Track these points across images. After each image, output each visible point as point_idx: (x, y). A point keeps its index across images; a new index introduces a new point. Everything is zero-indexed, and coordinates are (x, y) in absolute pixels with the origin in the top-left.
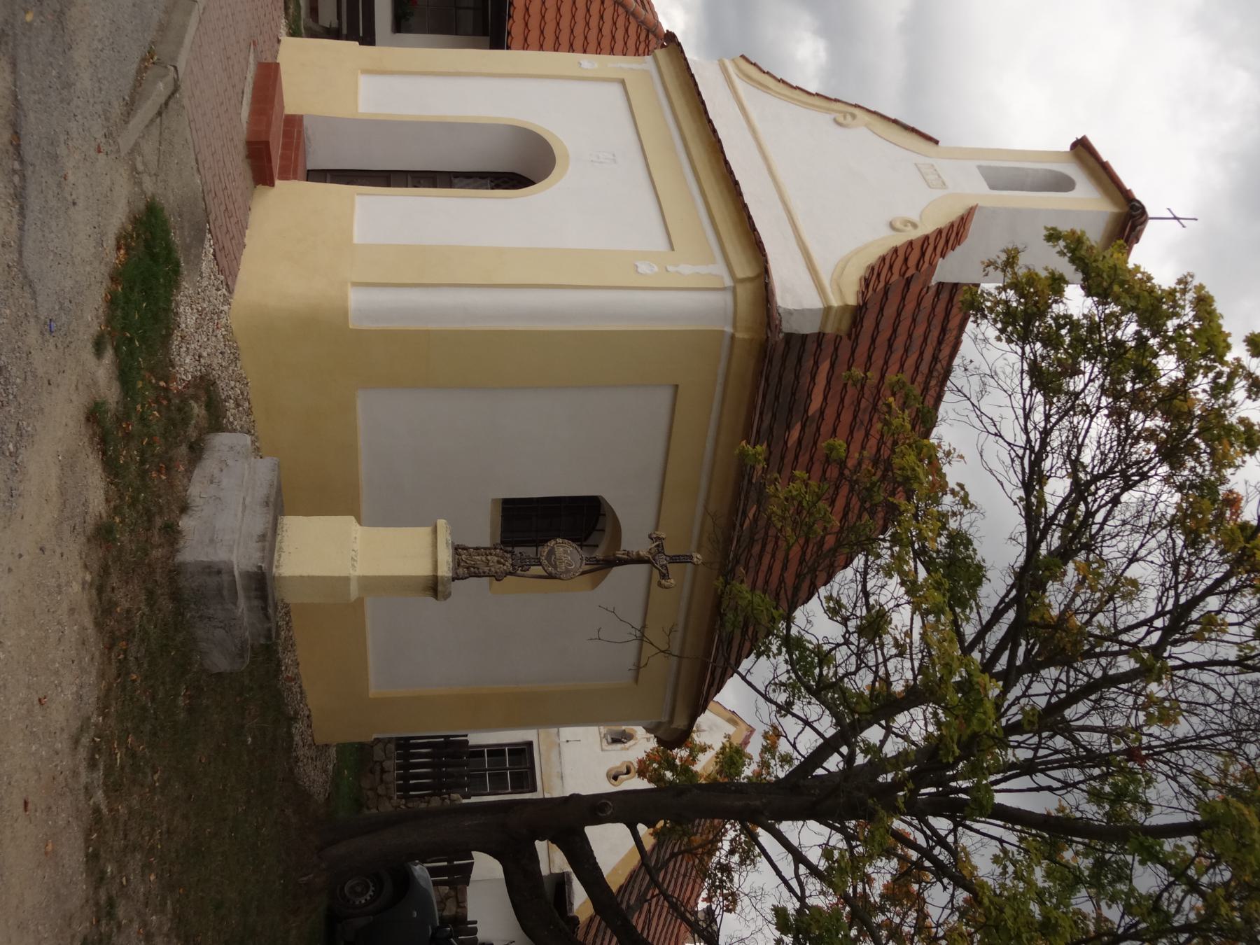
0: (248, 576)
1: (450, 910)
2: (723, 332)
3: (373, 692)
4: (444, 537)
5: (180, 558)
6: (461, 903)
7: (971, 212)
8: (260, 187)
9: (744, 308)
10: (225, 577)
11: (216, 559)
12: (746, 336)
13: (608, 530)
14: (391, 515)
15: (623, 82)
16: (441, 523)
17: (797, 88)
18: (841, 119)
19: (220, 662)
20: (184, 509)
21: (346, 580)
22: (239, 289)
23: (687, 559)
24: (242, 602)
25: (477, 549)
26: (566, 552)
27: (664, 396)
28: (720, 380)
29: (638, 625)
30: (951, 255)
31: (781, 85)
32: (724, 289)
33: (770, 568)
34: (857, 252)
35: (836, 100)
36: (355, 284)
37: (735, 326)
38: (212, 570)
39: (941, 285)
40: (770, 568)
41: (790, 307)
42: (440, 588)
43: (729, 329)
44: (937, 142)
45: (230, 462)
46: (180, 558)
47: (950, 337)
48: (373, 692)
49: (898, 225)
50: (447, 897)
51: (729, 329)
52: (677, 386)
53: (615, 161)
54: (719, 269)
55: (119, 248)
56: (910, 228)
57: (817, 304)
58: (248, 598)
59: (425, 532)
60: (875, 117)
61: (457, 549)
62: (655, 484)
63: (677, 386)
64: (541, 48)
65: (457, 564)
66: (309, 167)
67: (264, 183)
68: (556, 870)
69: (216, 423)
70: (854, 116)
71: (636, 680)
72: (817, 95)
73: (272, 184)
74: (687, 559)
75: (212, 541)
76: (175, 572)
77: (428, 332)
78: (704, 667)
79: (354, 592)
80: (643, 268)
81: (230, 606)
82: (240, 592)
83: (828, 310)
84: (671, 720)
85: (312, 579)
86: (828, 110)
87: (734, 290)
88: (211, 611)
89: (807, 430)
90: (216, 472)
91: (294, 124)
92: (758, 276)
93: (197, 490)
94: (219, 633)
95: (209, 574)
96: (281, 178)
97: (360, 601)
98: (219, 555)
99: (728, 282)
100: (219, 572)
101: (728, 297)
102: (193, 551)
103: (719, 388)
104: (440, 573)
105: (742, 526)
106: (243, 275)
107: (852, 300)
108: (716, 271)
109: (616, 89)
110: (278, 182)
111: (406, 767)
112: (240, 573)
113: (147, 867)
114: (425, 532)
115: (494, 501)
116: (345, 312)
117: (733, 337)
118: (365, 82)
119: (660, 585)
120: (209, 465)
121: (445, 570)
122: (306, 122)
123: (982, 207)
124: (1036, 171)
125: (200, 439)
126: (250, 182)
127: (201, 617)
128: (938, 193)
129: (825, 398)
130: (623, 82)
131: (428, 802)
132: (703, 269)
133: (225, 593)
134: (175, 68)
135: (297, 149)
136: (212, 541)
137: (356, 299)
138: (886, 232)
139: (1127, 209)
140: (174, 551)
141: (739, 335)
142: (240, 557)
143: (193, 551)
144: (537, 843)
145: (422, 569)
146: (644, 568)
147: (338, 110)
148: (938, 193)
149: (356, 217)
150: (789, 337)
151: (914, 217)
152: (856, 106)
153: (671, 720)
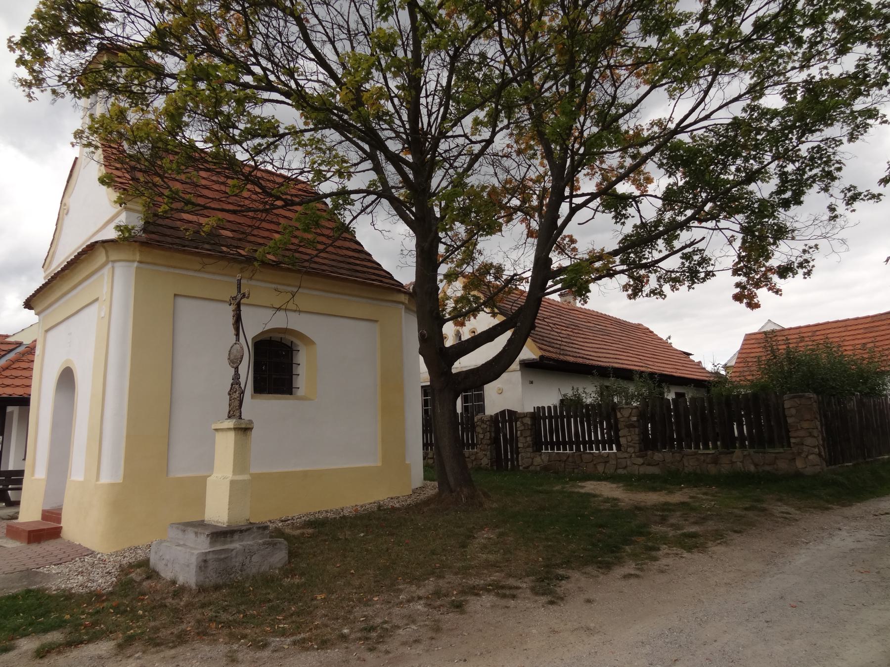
1: (528, 421)
2: (137, 268)
3: (379, 464)
6: (525, 415)
8: (61, 535)
9: (122, 256)
10: (210, 557)
11: (195, 563)
13: (282, 336)
21: (232, 483)
27: (181, 301)
28: (172, 270)
29: (271, 312)
32: (113, 267)
37: (133, 261)
38: (204, 564)
44: (76, 158)
46: (194, 586)
48: (379, 464)
50: (522, 422)
51: (136, 264)
52: (175, 295)
54: (106, 271)
58: (231, 542)
62: (206, 303)
63: (175, 295)
67: (60, 532)
68: (518, 367)
71: (376, 321)
76: (202, 589)
78: (308, 273)
81: (234, 553)
82: (226, 547)
84: (403, 303)
85: (230, 503)
86: (63, 219)
87: (114, 261)
88: (237, 564)
92: (104, 248)
94: (255, 558)
95: (206, 567)
97: (251, 475)
99: (110, 265)
101: (117, 265)
102: (188, 577)
103: (177, 271)
106: (89, 546)
109: (51, 334)
111: (558, 443)
112: (211, 547)
117: (140, 262)
119: (248, 298)
122: (47, 508)
126: (58, 541)
127: (241, 571)
130: (47, 331)
131: (630, 426)
132: (106, 277)
135: (52, 513)
137: (106, 479)
143: (188, 577)
144: (454, 371)
146: (242, 308)
150: (144, 230)
153: (403, 303)
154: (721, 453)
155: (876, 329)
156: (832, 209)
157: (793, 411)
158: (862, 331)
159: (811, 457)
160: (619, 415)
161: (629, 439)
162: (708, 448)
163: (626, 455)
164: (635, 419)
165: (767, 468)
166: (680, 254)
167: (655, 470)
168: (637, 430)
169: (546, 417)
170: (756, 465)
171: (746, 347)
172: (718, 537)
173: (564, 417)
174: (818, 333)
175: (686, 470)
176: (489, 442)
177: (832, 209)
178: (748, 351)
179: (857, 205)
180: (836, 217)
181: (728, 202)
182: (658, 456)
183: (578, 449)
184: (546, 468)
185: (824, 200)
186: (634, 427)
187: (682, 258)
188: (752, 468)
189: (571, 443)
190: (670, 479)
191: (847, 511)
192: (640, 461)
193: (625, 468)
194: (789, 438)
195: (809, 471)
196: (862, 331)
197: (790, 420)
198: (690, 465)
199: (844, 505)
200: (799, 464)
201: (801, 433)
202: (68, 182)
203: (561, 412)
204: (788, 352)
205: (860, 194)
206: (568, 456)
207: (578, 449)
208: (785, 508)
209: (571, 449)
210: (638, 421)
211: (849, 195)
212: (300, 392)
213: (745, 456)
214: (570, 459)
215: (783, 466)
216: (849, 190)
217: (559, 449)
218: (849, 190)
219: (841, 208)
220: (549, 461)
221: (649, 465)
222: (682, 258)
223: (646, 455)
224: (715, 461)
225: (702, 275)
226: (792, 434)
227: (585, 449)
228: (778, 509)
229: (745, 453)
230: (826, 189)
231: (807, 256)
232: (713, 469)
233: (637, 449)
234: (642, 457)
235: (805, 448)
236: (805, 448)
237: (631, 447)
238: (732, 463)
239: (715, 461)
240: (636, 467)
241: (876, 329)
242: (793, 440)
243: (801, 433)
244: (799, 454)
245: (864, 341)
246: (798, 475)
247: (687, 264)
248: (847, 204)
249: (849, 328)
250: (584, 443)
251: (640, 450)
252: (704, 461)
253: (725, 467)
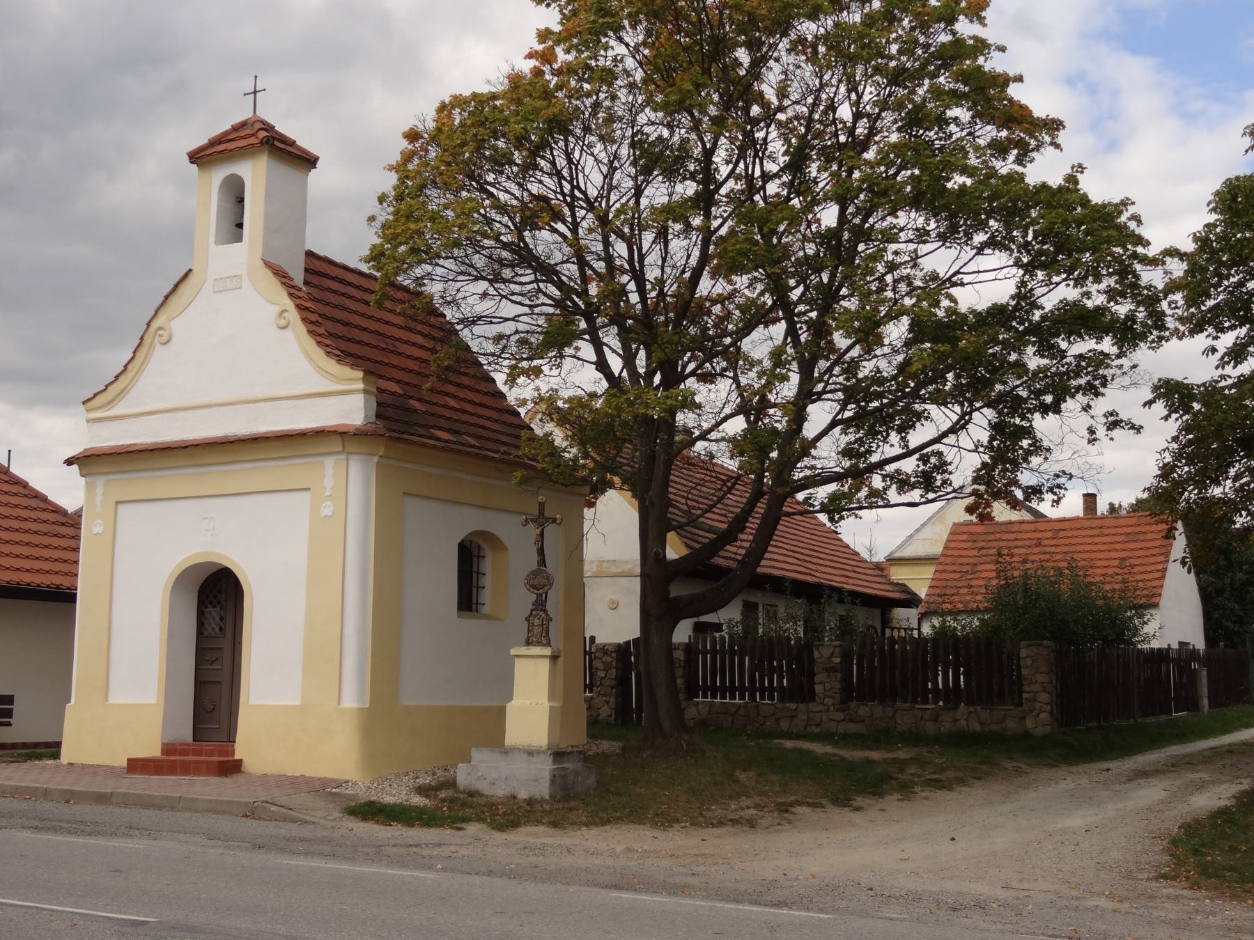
0: (554, 762)
4: (523, 650)
5: (547, 797)
14: (505, 685)
15: (118, 503)
16: (513, 652)
18: (164, 339)
20: (514, 797)
30: (291, 275)
33: (489, 419)
34: (311, 360)
35: (142, 338)
36: (339, 703)
40: (489, 419)
43: (376, 459)
46: (547, 797)
56: (285, 315)
59: (517, 662)
65: (539, 643)
69: (451, 784)
70: (160, 328)
73: (241, 761)
74: (542, 505)
75: (536, 780)
80: (327, 511)
83: (365, 391)
86: (151, 346)
91: (168, 749)
93: (500, 792)
94: (580, 779)
96: (233, 753)
98: (546, 775)
101: (352, 457)
105: (473, 446)
107: (360, 374)
108: (329, 463)
110: (237, 757)
111: (723, 690)
113: (709, 810)
114: (517, 662)
115: (459, 616)
116: (361, 709)
118: (118, 696)
120: (483, 787)
121: (547, 651)
125: (464, 792)
128: (246, 283)
129: (389, 379)
130: (118, 503)
131: (830, 670)
136: (536, 780)
138: (288, 333)
142: (545, 767)
145: (545, 665)
147: (158, 717)
152: (148, 324)
154: (942, 708)
155: (1142, 537)
156: (1091, 431)
157: (1029, 661)
158: (1121, 538)
159: (1043, 715)
160: (816, 654)
161: (828, 686)
162: (927, 703)
163: (821, 708)
164: (838, 660)
165: (995, 728)
166: (917, 456)
167: (854, 728)
168: (839, 675)
169: (707, 652)
170: (982, 724)
171: (953, 545)
172: (961, 782)
173: (707, 652)
174: (1062, 534)
175: (899, 728)
176: (614, 683)
177: (1091, 431)
178: (957, 553)
179: (1117, 433)
180: (1095, 440)
181: (974, 390)
182: (864, 710)
183: (753, 698)
184: (703, 724)
185: (1084, 421)
186: (835, 671)
187: (918, 460)
188: (978, 728)
189: (742, 690)
190: (882, 737)
191: (1073, 769)
192: (841, 716)
193: (819, 725)
194: (1021, 692)
195: (1040, 731)
196: (1121, 538)
197: (1024, 672)
198: (904, 721)
199: (1070, 765)
200: (1029, 723)
201: (1035, 688)
202: (167, 298)
203: (731, 646)
204: (1026, 577)
205: (1122, 421)
206: (739, 707)
207: (753, 698)
208: (1015, 764)
209: (742, 698)
210: (841, 663)
211: (1110, 419)
212: (486, 610)
213: (970, 713)
214: (742, 712)
215: (1011, 725)
216: (1111, 415)
217: (723, 697)
218: (1111, 415)
219: (1101, 432)
220: (709, 713)
221: (851, 721)
222: (918, 460)
223: (849, 708)
224: (935, 719)
225: (938, 483)
226: (1025, 688)
227: (762, 698)
228: (1009, 765)
229: (971, 709)
230: (1087, 408)
231: (1062, 480)
232: (930, 728)
233: (838, 701)
234: (843, 711)
235: (1037, 705)
236: (1037, 705)
237: (829, 697)
238: (955, 720)
239: (935, 719)
240: (834, 725)
241: (1142, 537)
242: (1025, 696)
243: (1035, 688)
244: (1031, 711)
245: (1123, 555)
246: (1027, 735)
247: (922, 467)
248: (1109, 429)
249: (1106, 531)
250: (763, 690)
251: (842, 702)
252: (922, 718)
253: (946, 725)
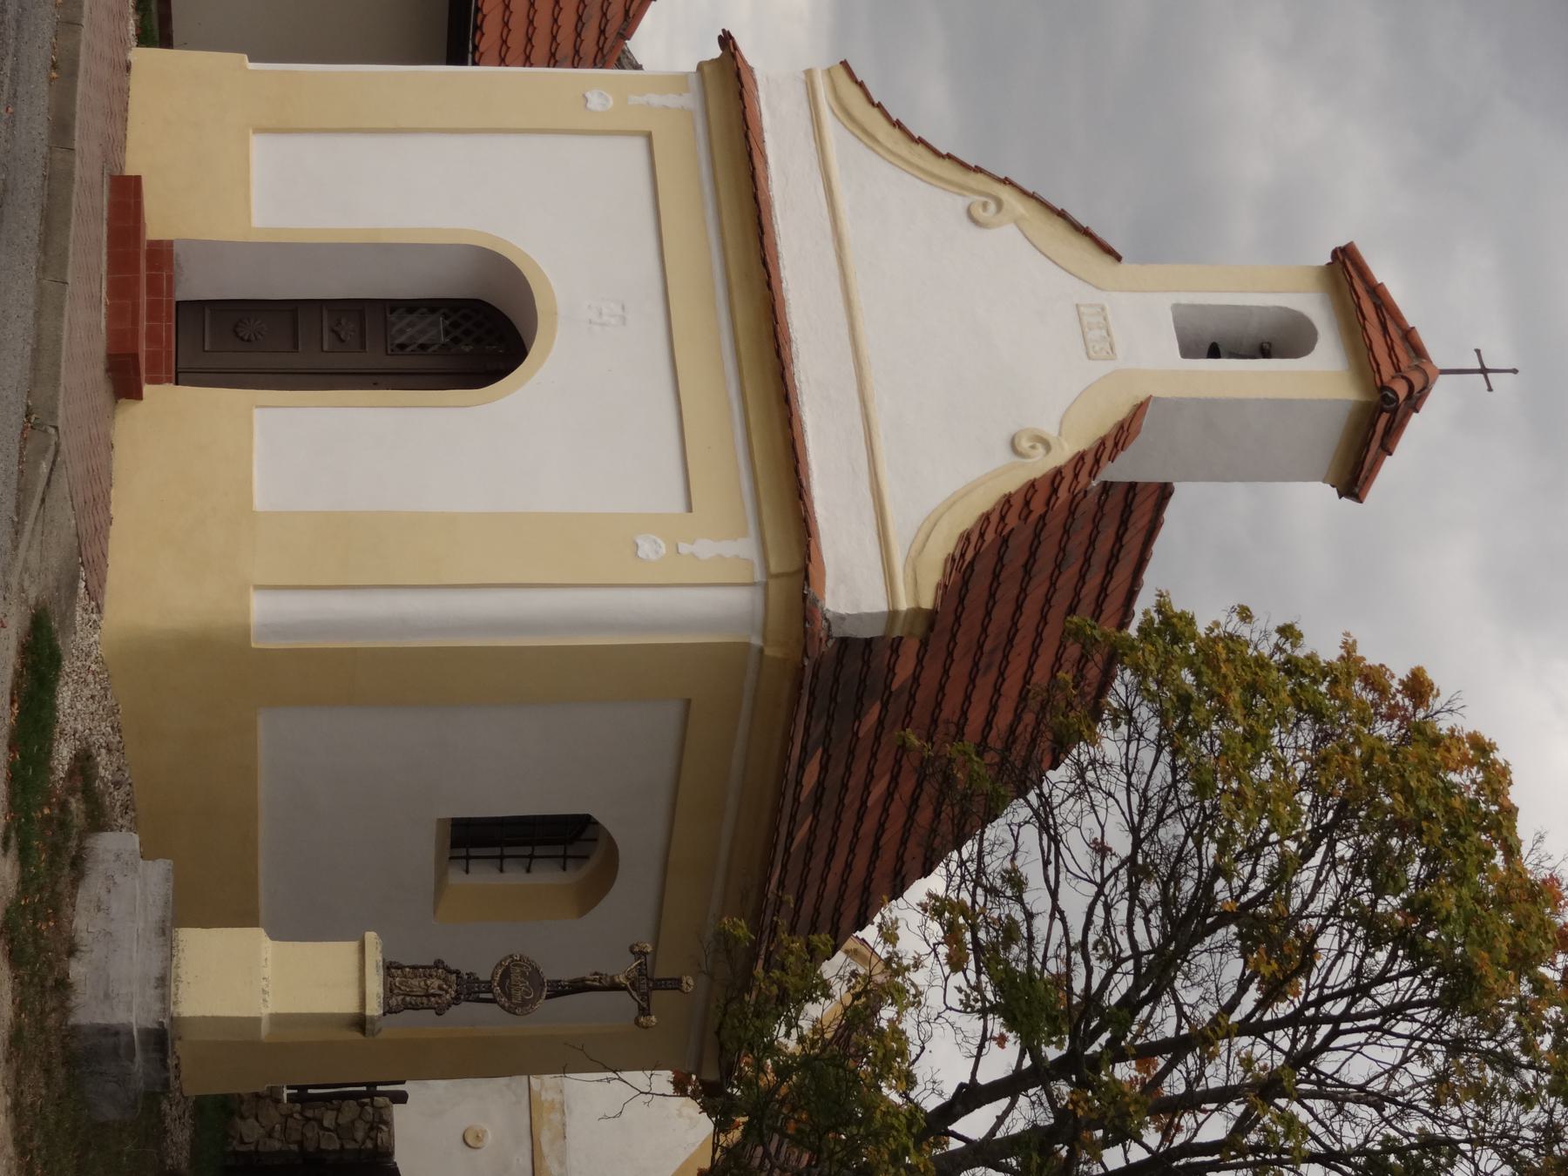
0: (146, 1032)
2: (747, 645)
4: (374, 957)
5: (72, 1021)
7: (1140, 409)
11: (114, 1021)
12: (779, 655)
15: (649, 137)
16: (371, 937)
17: (920, 141)
19: (109, 1112)
20: (72, 951)
21: (256, 1021)
22: (108, 610)
23: (675, 984)
24: (139, 1058)
25: (414, 968)
26: (547, 877)
31: (896, 132)
32: (753, 584)
34: (950, 504)
35: (978, 170)
36: (258, 587)
39: (1107, 487)
40: (848, 866)
41: (842, 611)
42: (368, 1026)
43: (756, 641)
45: (118, 879)
46: (72, 1021)
47: (1133, 539)
49: (1024, 444)
52: (688, 702)
53: (624, 320)
55: (12, 703)
56: (1041, 449)
57: (882, 606)
59: (350, 947)
60: (1033, 203)
61: (389, 968)
64: (527, 61)
65: (389, 990)
66: (181, 294)
69: (98, 822)
70: (1000, 204)
72: (949, 156)
73: (138, 395)
74: (675, 984)
75: (107, 996)
77: (354, 650)
79: (265, 1029)
83: (893, 614)
86: (963, 188)
87: (766, 586)
89: (891, 707)
90: (103, 892)
91: (162, 253)
93: (83, 923)
99: (758, 576)
100: (117, 1033)
101: (758, 595)
104: (368, 1012)
107: (927, 602)
108: (744, 548)
109: (639, 144)
110: (147, 389)
116: (246, 631)
117: (761, 651)
121: (374, 1008)
122: (176, 248)
123: (1158, 398)
124: (1266, 309)
128: (1102, 368)
130: (649, 137)
133: (122, 1052)
134: (56, 428)
136: (107, 996)
138: (1003, 457)
139: (1378, 397)
140: (64, 1010)
141: (768, 652)
142: (132, 1012)
143: (88, 1011)
145: (345, 1004)
147: (223, 230)
148: (1102, 368)
149: (255, 456)
151: (1050, 430)
152: (1006, 181)
